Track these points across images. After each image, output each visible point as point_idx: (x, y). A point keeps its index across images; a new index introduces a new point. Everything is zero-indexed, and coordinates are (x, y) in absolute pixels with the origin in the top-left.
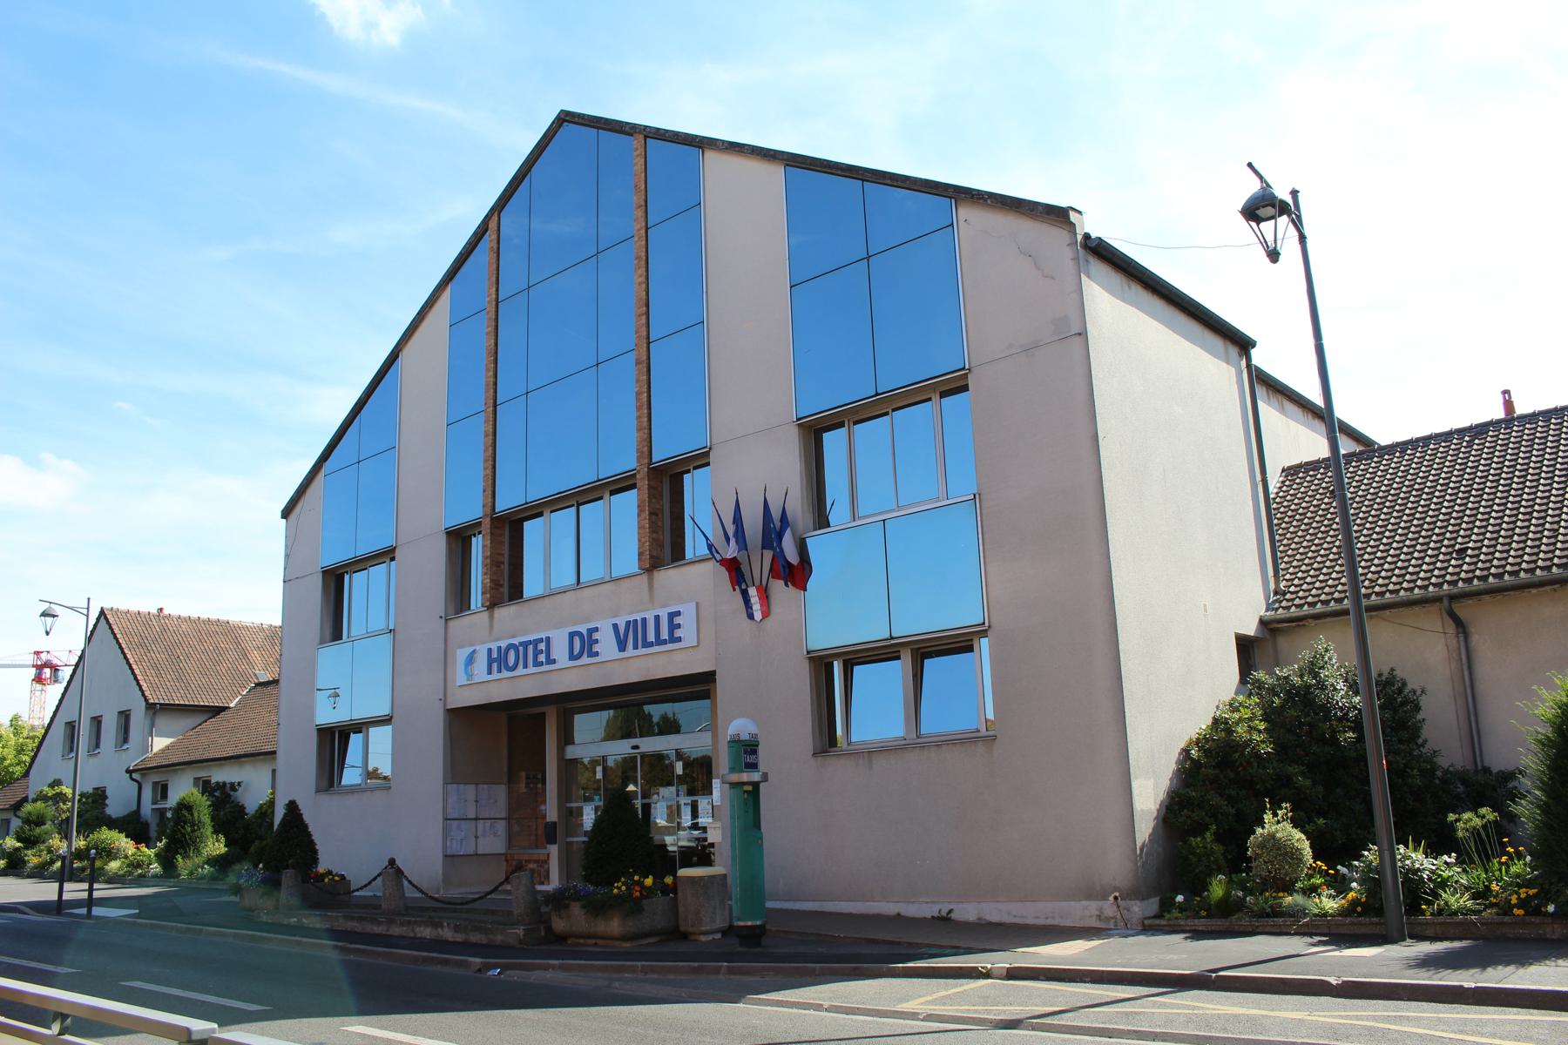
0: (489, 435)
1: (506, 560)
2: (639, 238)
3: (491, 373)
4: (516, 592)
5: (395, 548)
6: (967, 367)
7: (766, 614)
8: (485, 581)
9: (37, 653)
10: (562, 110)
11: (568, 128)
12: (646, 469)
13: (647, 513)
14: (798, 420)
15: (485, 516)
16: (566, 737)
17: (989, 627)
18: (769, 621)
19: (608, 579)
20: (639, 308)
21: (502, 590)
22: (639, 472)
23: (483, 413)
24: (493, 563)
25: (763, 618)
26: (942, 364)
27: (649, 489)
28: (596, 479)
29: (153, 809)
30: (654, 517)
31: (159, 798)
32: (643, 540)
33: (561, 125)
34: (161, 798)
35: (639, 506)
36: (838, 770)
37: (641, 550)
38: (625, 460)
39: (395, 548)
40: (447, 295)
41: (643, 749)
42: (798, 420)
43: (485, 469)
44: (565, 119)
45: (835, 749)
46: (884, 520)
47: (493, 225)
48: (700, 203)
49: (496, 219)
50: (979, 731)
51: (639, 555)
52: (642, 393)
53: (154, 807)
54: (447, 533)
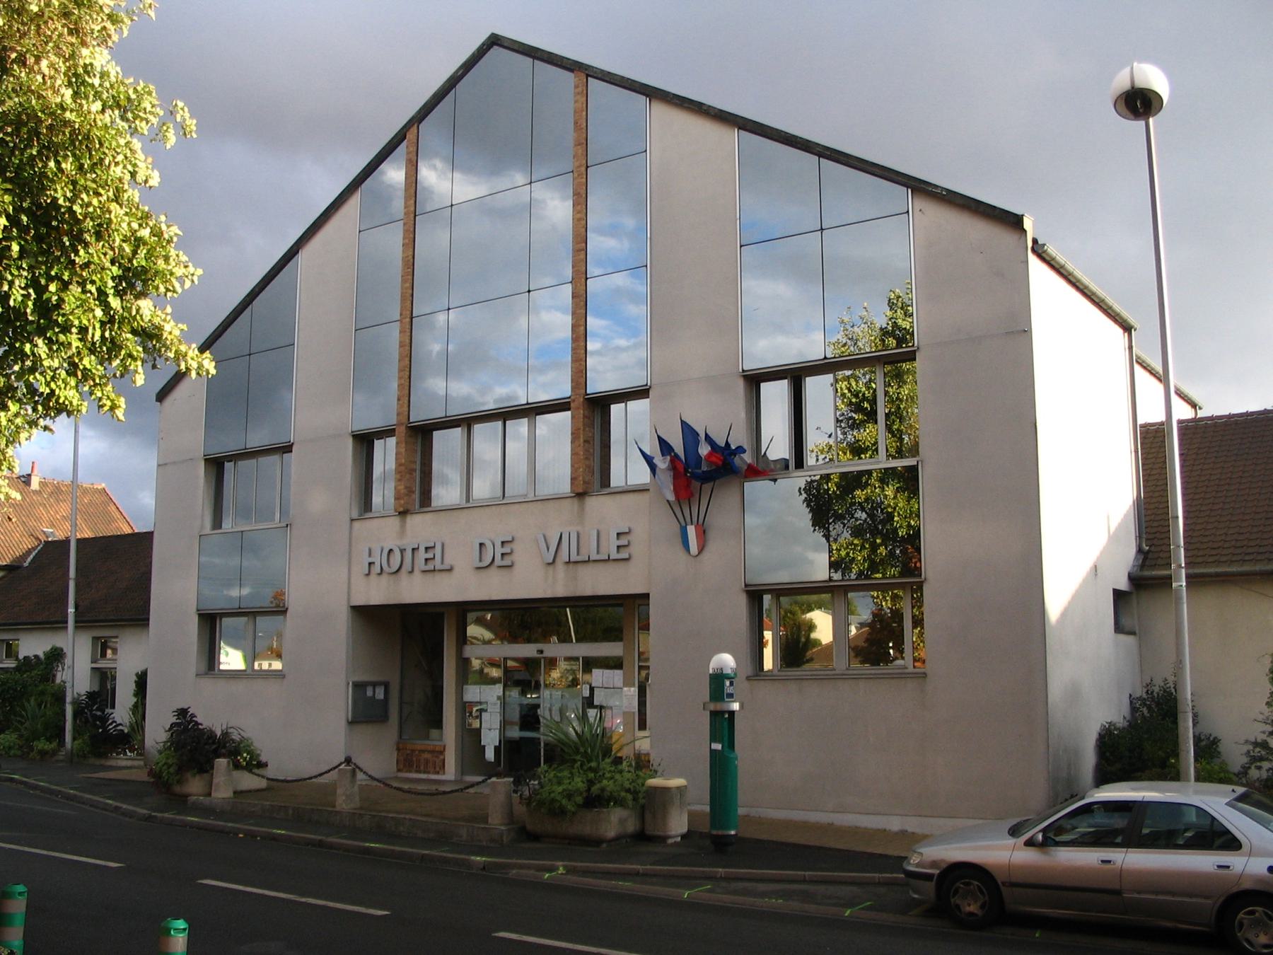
0: (405, 346)
1: (418, 467)
2: (579, 175)
3: (408, 285)
4: (426, 498)
5: (293, 444)
6: (649, 384)
7: (701, 550)
8: (399, 488)
9: (45, 479)
10: (493, 34)
11: (496, 50)
12: (582, 400)
13: (582, 440)
14: (352, 432)
15: (399, 424)
16: (462, 639)
17: (925, 579)
18: (706, 555)
19: (531, 497)
20: (578, 243)
21: (414, 496)
22: (574, 401)
23: (398, 323)
24: (403, 470)
25: (699, 554)
26: (279, 440)
27: (583, 418)
28: (444, 415)
29: (92, 668)
30: (587, 445)
31: (4, 657)
32: (576, 466)
33: (492, 47)
34: (6, 657)
35: (572, 434)
36: (208, 684)
37: (573, 476)
38: (563, 390)
39: (293, 444)
40: (355, 201)
41: (545, 654)
42: (205, 456)
43: (400, 378)
44: (495, 41)
45: (212, 672)
46: (242, 532)
47: (411, 135)
48: (646, 151)
49: (416, 131)
50: (906, 668)
51: (571, 479)
52: (580, 326)
53: (94, 665)
54: (206, 460)
